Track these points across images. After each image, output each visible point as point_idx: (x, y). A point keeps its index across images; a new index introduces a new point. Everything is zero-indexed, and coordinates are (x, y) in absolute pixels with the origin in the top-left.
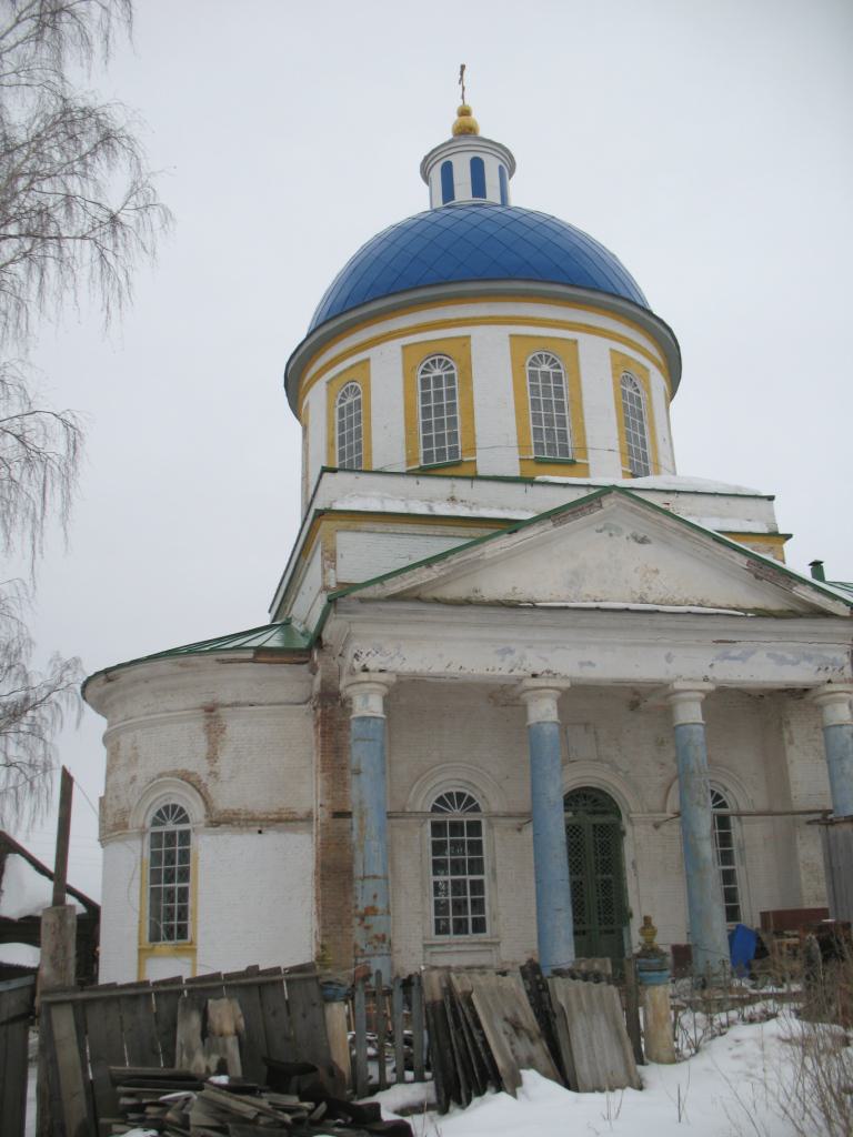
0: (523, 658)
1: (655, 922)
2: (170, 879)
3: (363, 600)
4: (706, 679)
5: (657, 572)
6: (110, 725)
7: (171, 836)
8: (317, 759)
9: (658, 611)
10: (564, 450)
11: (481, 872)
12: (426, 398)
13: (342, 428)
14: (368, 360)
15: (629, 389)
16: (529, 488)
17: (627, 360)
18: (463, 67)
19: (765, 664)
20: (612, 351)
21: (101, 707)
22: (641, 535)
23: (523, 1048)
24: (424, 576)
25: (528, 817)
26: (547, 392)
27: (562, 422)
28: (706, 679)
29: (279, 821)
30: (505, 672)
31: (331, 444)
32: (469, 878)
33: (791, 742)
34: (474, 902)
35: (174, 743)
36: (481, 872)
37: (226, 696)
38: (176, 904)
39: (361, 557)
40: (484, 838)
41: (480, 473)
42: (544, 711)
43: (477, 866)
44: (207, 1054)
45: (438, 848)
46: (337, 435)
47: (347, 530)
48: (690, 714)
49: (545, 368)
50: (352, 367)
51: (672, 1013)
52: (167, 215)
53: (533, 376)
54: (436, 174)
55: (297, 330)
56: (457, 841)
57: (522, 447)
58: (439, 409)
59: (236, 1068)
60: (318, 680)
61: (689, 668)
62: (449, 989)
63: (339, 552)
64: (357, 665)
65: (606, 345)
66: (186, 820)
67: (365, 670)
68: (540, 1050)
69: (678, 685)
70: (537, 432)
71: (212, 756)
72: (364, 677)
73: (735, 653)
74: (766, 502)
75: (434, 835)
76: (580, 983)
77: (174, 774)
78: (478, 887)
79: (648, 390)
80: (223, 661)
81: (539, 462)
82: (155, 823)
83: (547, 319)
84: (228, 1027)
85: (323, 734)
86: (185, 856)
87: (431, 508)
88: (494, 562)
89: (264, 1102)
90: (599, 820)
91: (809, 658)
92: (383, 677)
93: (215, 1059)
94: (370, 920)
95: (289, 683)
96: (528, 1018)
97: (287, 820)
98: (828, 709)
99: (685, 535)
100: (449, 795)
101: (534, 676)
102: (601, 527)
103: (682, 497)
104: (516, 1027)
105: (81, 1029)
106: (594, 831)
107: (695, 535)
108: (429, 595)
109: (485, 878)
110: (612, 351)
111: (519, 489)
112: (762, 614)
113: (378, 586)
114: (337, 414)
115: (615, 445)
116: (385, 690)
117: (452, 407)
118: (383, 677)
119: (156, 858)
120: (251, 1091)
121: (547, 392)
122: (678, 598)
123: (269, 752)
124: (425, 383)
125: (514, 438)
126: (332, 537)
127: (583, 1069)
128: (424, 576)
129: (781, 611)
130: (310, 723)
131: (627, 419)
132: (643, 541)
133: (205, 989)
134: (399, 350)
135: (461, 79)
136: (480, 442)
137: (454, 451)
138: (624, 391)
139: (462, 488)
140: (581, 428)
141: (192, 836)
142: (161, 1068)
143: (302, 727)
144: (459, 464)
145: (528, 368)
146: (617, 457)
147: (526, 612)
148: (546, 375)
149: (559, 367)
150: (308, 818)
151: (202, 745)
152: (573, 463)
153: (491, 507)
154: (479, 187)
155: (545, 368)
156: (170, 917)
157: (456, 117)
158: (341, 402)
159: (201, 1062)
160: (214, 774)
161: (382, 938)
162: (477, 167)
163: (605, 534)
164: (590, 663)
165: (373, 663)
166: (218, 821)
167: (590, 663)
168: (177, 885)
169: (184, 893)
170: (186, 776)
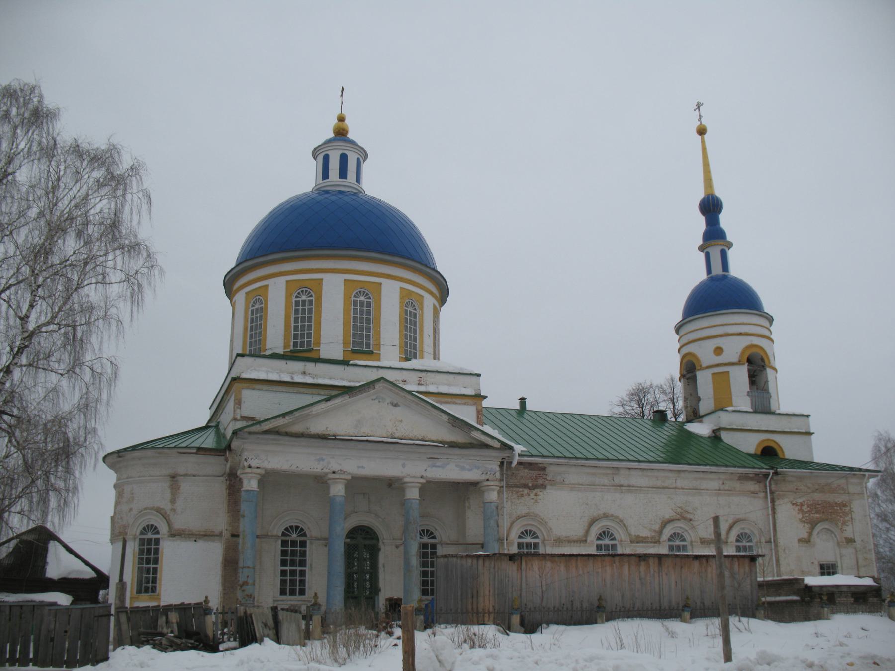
0: (329, 463)
1: (318, 595)
2: (148, 562)
3: (250, 433)
4: (422, 477)
5: (401, 421)
6: (118, 479)
7: (149, 541)
8: (225, 505)
9: (398, 443)
10: (368, 345)
11: (305, 566)
12: (297, 311)
13: (252, 322)
14: (268, 286)
15: (410, 309)
16: (346, 367)
17: (410, 293)
18: (343, 89)
19: (454, 469)
20: (401, 288)
21: (112, 466)
22: (395, 402)
23: (267, 631)
24: (281, 422)
25: (327, 541)
26: (362, 312)
27: (369, 329)
28: (422, 477)
29: (205, 535)
30: (319, 470)
31: (245, 329)
32: (299, 568)
33: (469, 508)
34: (300, 581)
35: (152, 493)
36: (305, 566)
37: (181, 470)
38: (151, 575)
39: (257, 404)
40: (307, 549)
41: (322, 357)
42: (338, 490)
43: (303, 563)
44: (168, 628)
45: (284, 553)
46: (249, 325)
47: (248, 388)
48: (413, 494)
49: (362, 298)
50: (259, 288)
51: (304, 623)
52: (162, 271)
53: (355, 303)
54: (320, 158)
55: (231, 263)
56: (293, 550)
57: (345, 343)
58: (303, 319)
59: (176, 633)
60: (228, 465)
61: (413, 470)
62: (245, 613)
63: (243, 400)
64: (246, 464)
65: (398, 285)
66: (158, 533)
67: (250, 467)
68: (272, 633)
69: (406, 480)
70: (354, 335)
71: (173, 501)
72: (249, 470)
73: (438, 463)
74: (475, 378)
75: (282, 546)
76: (289, 613)
77: (152, 509)
78: (303, 573)
79: (422, 309)
80: (181, 453)
81: (354, 352)
82: (142, 533)
83: (365, 270)
84: (174, 621)
85: (229, 494)
86: (157, 551)
87: (292, 378)
88: (317, 415)
89: (184, 640)
90: (367, 542)
91: (478, 468)
92: (258, 471)
93: (169, 630)
94: (244, 587)
95: (215, 465)
96: (271, 622)
97: (210, 536)
98: (486, 493)
99: (417, 404)
100: (291, 527)
101: (334, 472)
102: (374, 397)
103: (429, 374)
104: (266, 625)
105: (129, 619)
106: (362, 545)
107: (423, 404)
108: (284, 430)
109: (307, 569)
110: (401, 288)
111: (339, 368)
112: (453, 445)
113: (258, 426)
114: (250, 313)
115: (397, 342)
116: (259, 477)
117: (310, 319)
118: (258, 471)
119: (141, 552)
120: (181, 638)
121: (362, 312)
122: (411, 435)
123: (200, 500)
124: (297, 303)
125: (341, 338)
126: (240, 392)
127: (284, 637)
128: (281, 422)
129: (465, 444)
130: (224, 487)
131: (406, 326)
132: (396, 405)
133: (168, 609)
134: (285, 283)
135: (341, 96)
136: (323, 340)
137: (309, 343)
138: (406, 311)
139: (310, 367)
140: (378, 333)
141: (161, 542)
142: (153, 631)
143: (220, 488)
144: (311, 351)
145: (353, 298)
146: (397, 350)
147: (331, 441)
148: (362, 303)
149: (370, 298)
150: (220, 535)
151: (168, 494)
152: (372, 353)
153: (325, 378)
154: (343, 174)
155: (362, 298)
156: (148, 581)
157: (336, 121)
158: (253, 306)
159: (165, 630)
160: (173, 510)
161: (250, 596)
162: (344, 159)
163: (377, 401)
164: (363, 467)
165: (254, 463)
166: (175, 534)
167: (363, 467)
168: (151, 566)
169: (155, 570)
170: (159, 511)
